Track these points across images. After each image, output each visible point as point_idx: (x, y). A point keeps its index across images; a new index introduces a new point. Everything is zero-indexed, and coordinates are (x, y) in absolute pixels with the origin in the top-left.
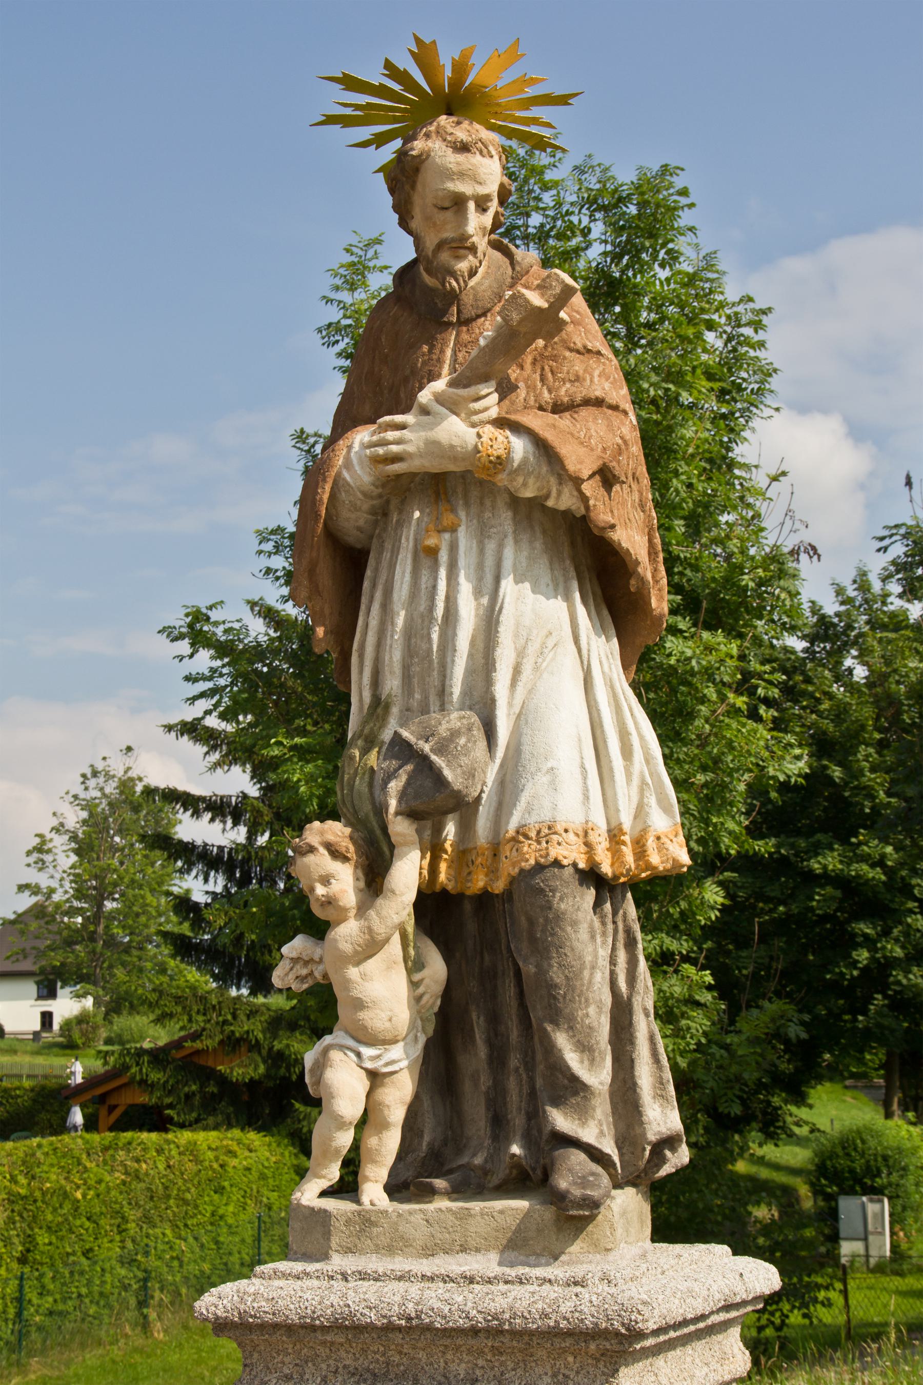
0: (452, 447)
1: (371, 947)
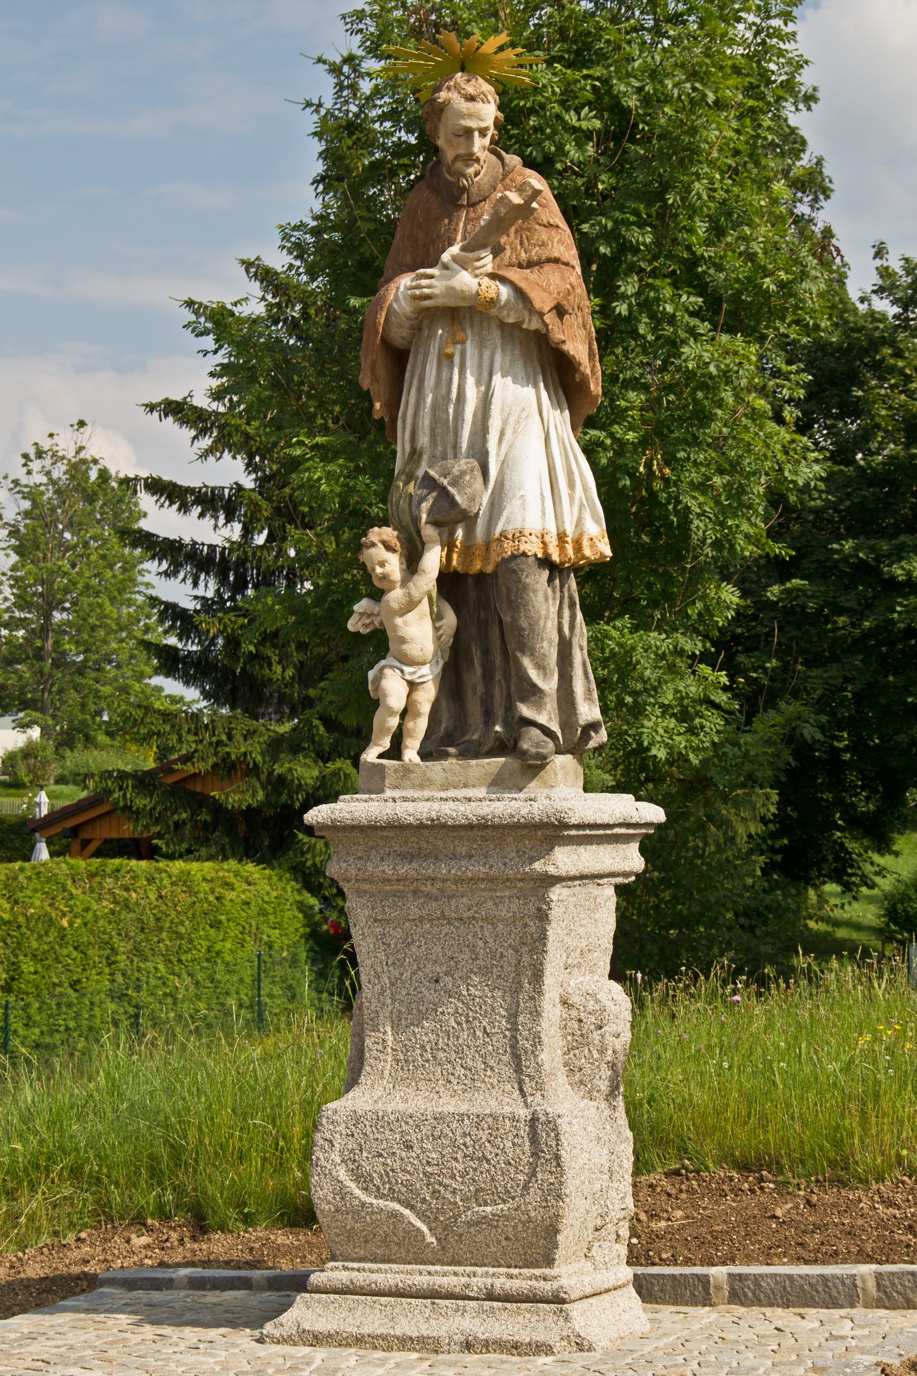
0: (462, 291)
1: (410, 605)
